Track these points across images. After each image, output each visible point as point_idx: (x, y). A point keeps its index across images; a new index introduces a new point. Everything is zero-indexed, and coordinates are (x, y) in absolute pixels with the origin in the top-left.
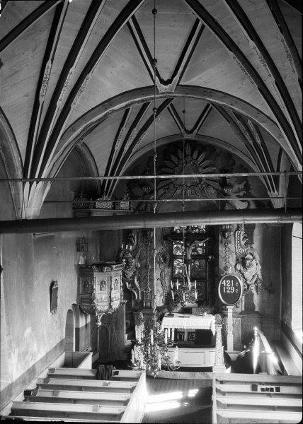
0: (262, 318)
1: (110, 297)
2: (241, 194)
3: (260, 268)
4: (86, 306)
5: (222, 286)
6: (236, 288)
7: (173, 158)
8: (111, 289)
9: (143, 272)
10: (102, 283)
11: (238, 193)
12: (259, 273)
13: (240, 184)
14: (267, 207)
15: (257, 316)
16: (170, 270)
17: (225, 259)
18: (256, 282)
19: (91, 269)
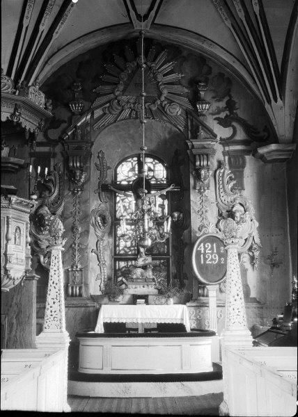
0: (262, 308)
2: (222, 115)
3: (257, 224)
5: (199, 253)
6: (220, 255)
11: (218, 113)
12: (256, 234)
13: (219, 101)
15: (254, 305)
17: (201, 213)
18: (250, 249)
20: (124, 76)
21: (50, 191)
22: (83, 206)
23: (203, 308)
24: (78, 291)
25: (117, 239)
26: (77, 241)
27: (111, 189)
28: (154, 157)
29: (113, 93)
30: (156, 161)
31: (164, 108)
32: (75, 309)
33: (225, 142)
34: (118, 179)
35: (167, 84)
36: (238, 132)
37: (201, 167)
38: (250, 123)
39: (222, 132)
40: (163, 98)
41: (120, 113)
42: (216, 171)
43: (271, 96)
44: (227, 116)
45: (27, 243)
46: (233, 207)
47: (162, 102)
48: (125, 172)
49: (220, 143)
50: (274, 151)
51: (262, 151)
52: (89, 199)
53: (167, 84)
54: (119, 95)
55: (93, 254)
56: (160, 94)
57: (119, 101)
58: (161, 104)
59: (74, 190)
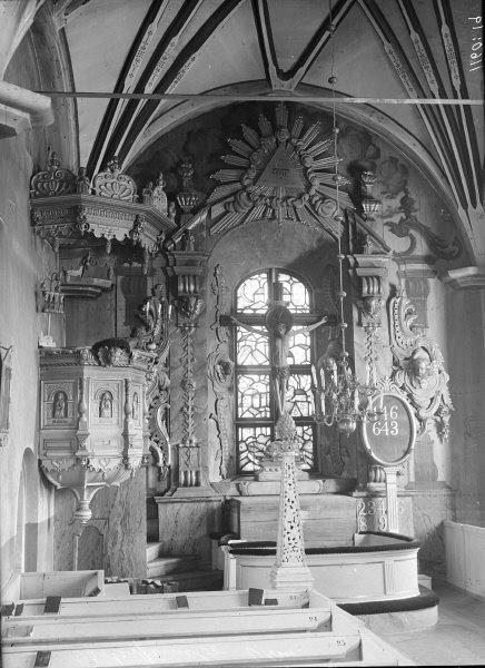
1: (125, 435)
2: (396, 219)
4: (59, 462)
7: (249, 133)
8: (127, 414)
9: (178, 396)
10: (104, 398)
11: (390, 216)
12: (445, 391)
14: (451, 248)
16: (232, 397)
18: (437, 414)
19: (78, 355)
20: (258, 159)
21: (148, 328)
22: (198, 349)
23: (376, 499)
24: (194, 478)
25: (240, 395)
26: (190, 403)
27: (231, 320)
28: (292, 274)
29: (240, 181)
30: (294, 279)
31: (313, 206)
32: (190, 505)
33: (401, 258)
34: (239, 306)
35: (319, 171)
36: (418, 246)
37: (370, 297)
38: (433, 230)
39: (398, 244)
40: (313, 192)
41: (250, 211)
42: (389, 301)
43: (468, 198)
44: (402, 220)
45: (144, 414)
46: (414, 353)
47: (311, 197)
48: (252, 294)
49: (393, 260)
50: (471, 276)
51: (455, 275)
52: (205, 340)
53: (319, 171)
54: (249, 185)
55: (212, 421)
56: (309, 186)
57: (248, 195)
58: (310, 201)
59: (185, 326)
